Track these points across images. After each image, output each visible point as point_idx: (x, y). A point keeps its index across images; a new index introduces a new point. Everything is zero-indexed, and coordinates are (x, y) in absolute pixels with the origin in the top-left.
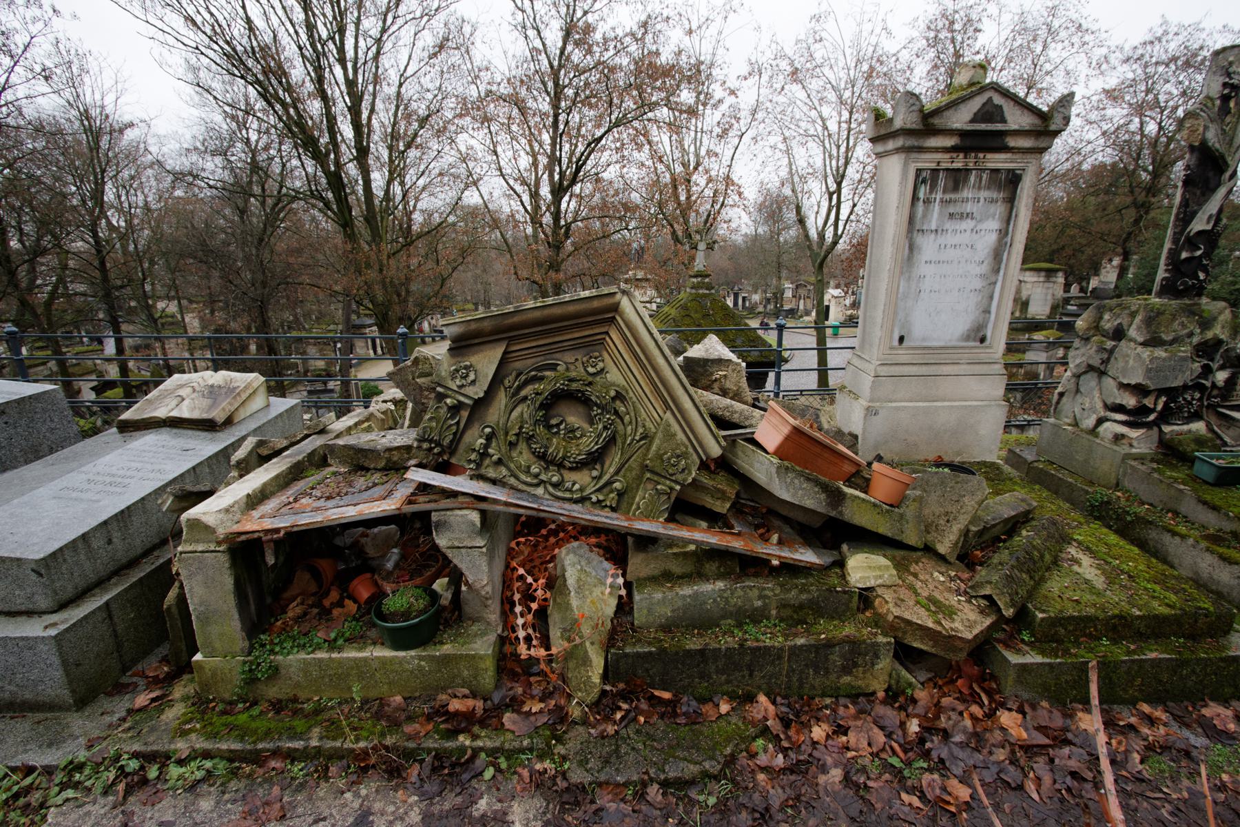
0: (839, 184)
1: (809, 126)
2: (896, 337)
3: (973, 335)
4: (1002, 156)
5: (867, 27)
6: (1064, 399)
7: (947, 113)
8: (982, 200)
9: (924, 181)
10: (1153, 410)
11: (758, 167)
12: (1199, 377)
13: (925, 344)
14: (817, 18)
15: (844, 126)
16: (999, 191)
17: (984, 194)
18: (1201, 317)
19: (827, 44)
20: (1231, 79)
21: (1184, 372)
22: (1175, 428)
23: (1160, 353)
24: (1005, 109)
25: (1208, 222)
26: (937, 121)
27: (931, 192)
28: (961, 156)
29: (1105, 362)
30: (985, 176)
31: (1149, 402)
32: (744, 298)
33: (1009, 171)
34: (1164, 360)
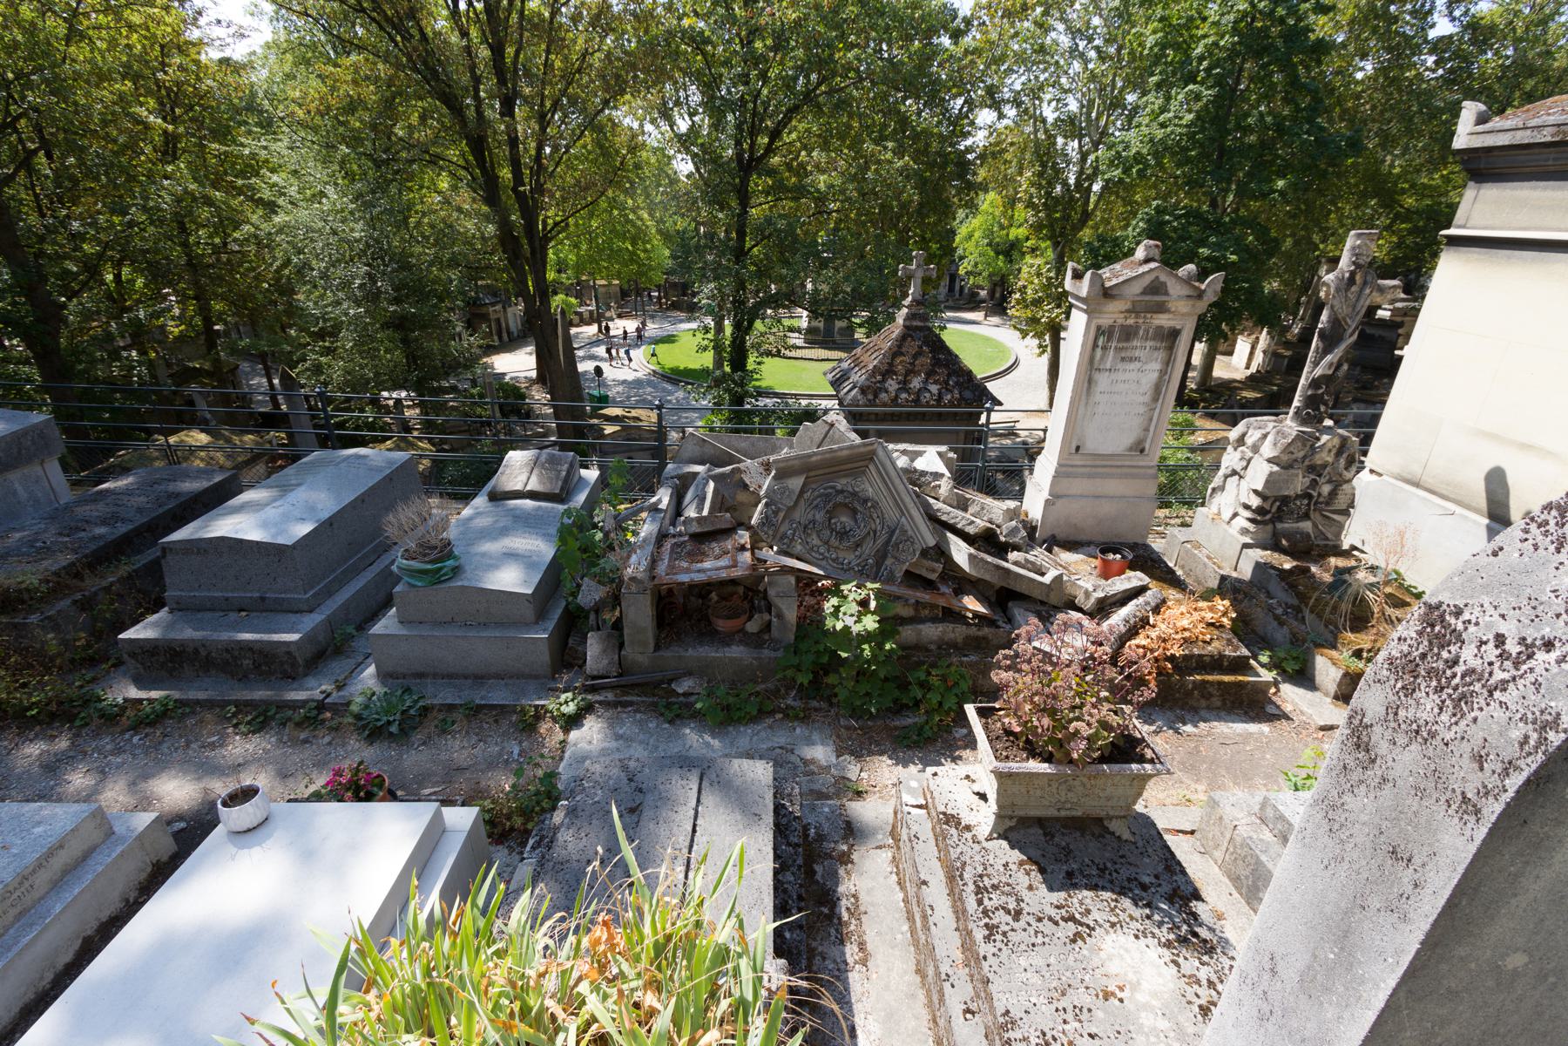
17: (1149, 344)
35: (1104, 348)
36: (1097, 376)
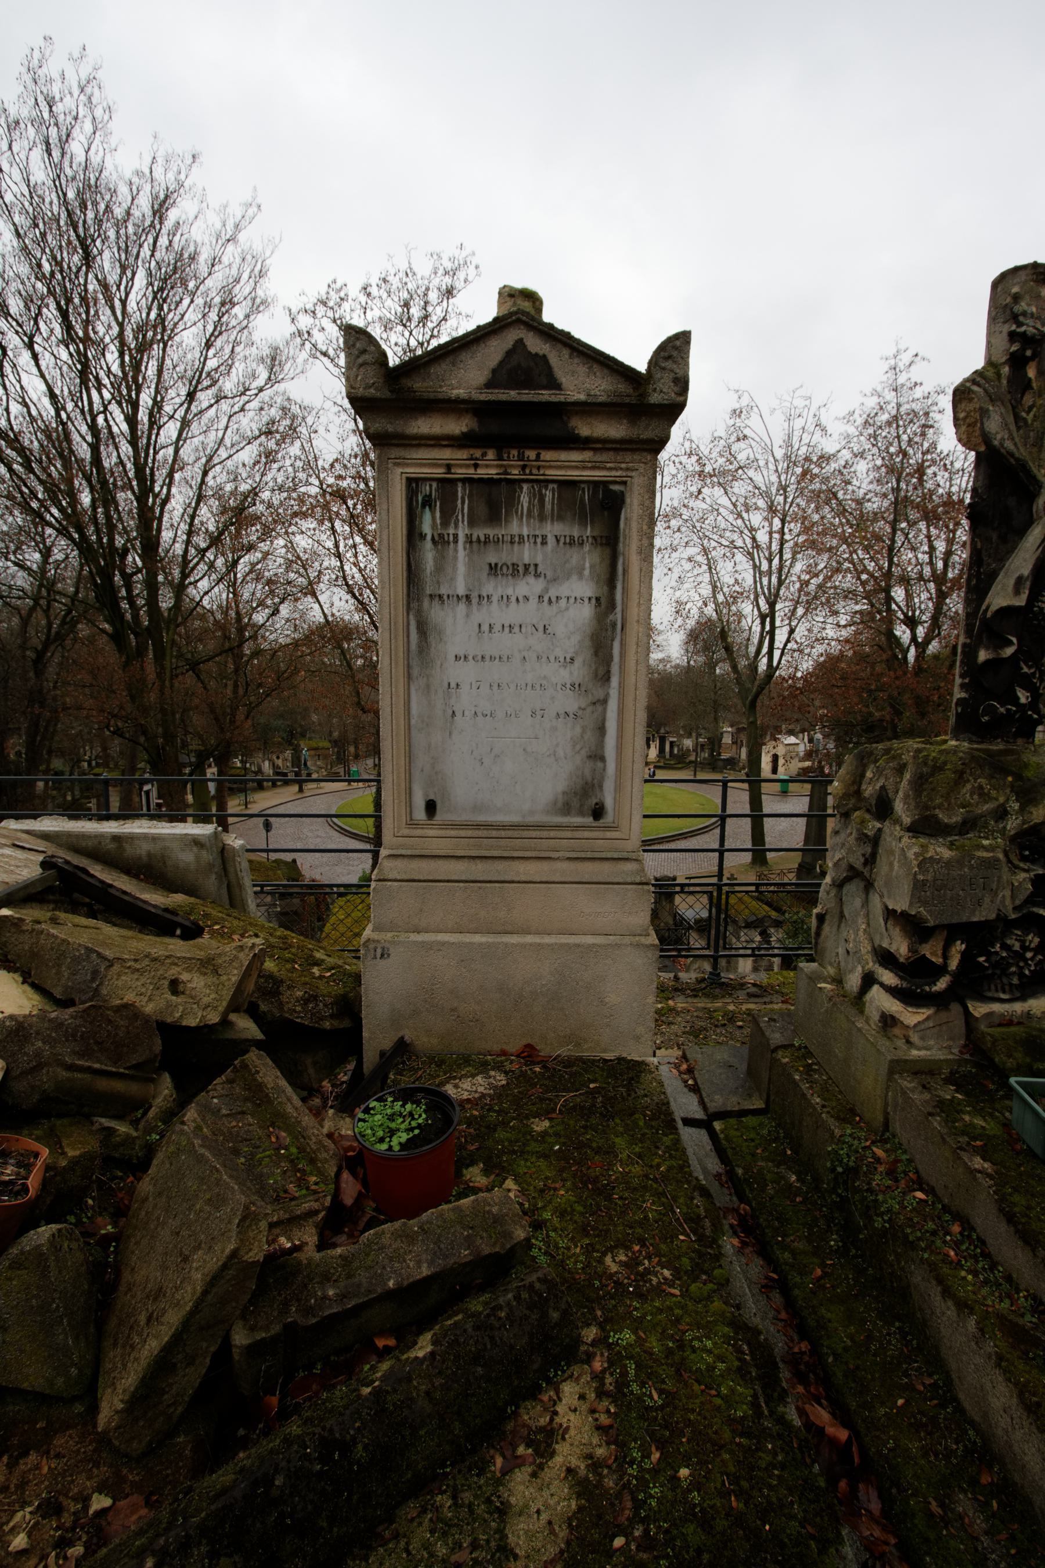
0: (772, 605)
1: (735, 536)
2: (419, 803)
3: (575, 803)
4: (575, 456)
5: (798, 423)
6: (826, 928)
7: (435, 370)
8: (551, 540)
9: (428, 502)
10: (942, 970)
11: (674, 584)
12: (1030, 901)
13: (481, 818)
14: (737, 413)
15: (776, 536)
16: (583, 523)
17: (552, 529)
18: (1018, 777)
19: (753, 444)
20: (1020, 324)
21: (994, 893)
22: (996, 1007)
23: (941, 850)
24: (554, 360)
25: (1017, 591)
26: (418, 385)
27: (445, 524)
28: (491, 454)
29: (871, 860)
30: (548, 495)
31: (931, 951)
32: (672, 743)
33: (595, 484)
34: (948, 864)
35: (440, 541)
36: (436, 613)
